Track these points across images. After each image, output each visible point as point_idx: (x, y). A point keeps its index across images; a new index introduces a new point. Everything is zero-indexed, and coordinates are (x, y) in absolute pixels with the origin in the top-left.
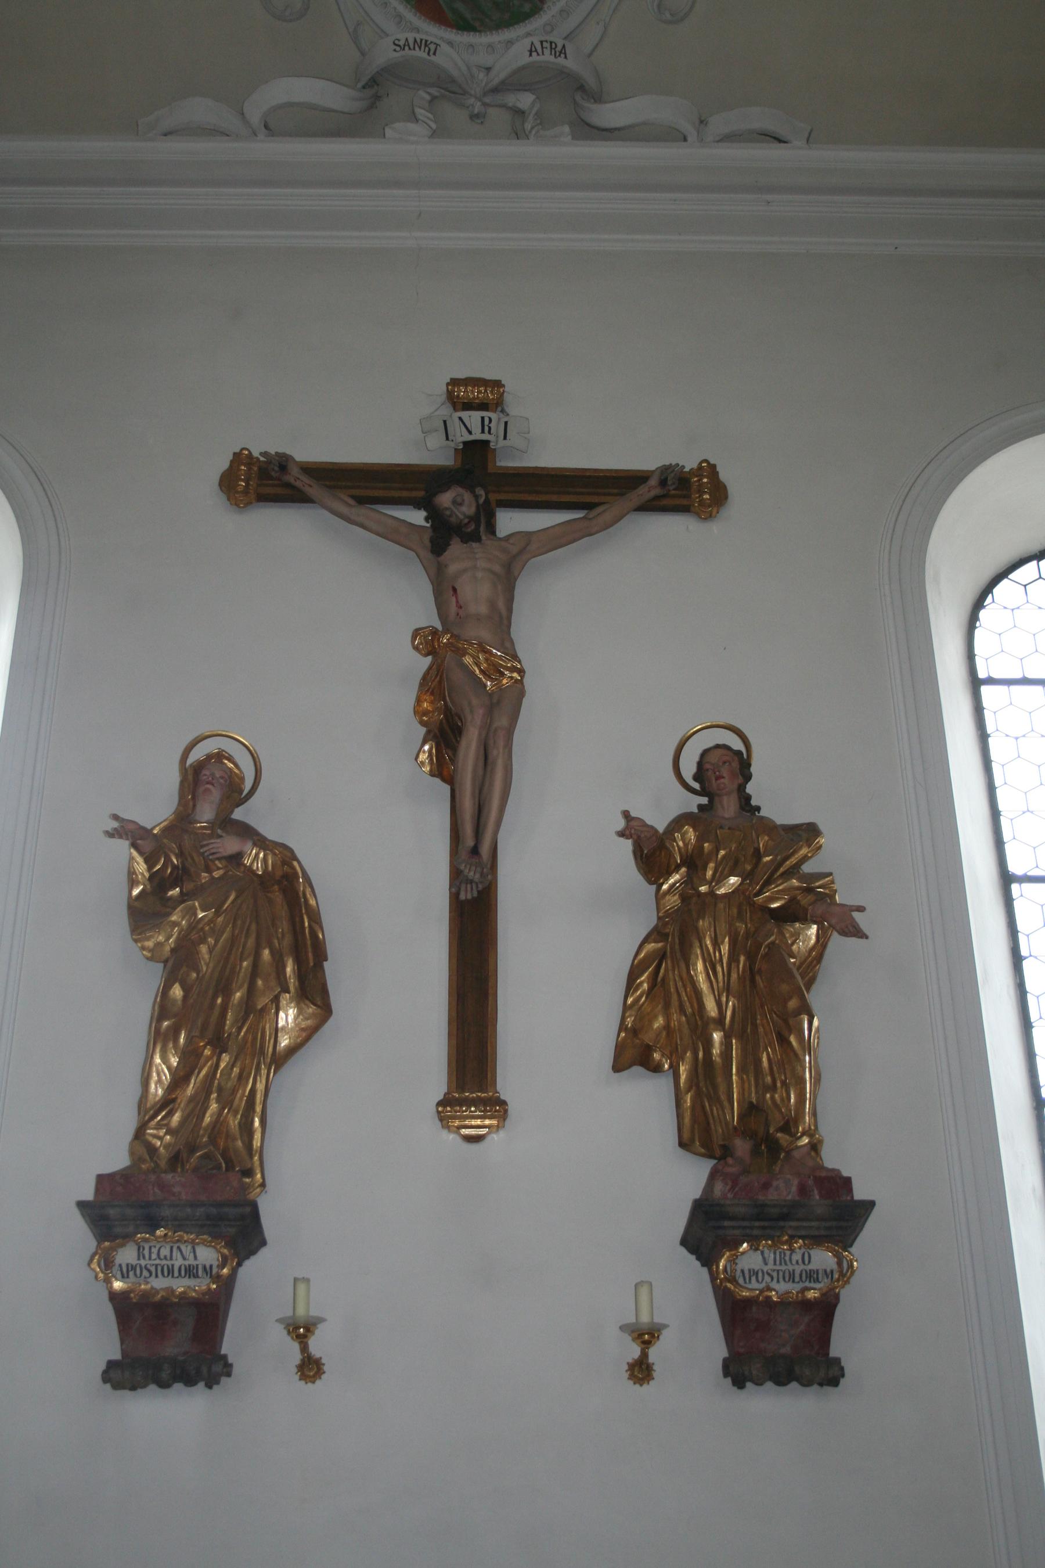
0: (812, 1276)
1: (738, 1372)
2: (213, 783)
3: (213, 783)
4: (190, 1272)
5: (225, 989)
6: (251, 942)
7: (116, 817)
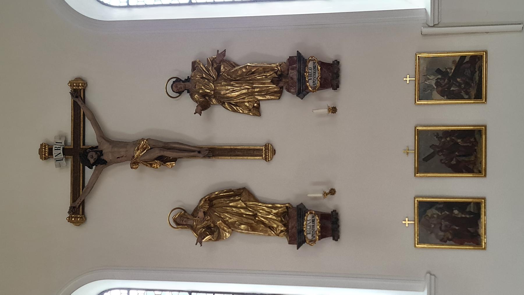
0: (314, 67)
1: (336, 86)
2: (183, 219)
3: (183, 219)
4: (313, 221)
5: (241, 215)
6: (228, 208)
7: (196, 244)
